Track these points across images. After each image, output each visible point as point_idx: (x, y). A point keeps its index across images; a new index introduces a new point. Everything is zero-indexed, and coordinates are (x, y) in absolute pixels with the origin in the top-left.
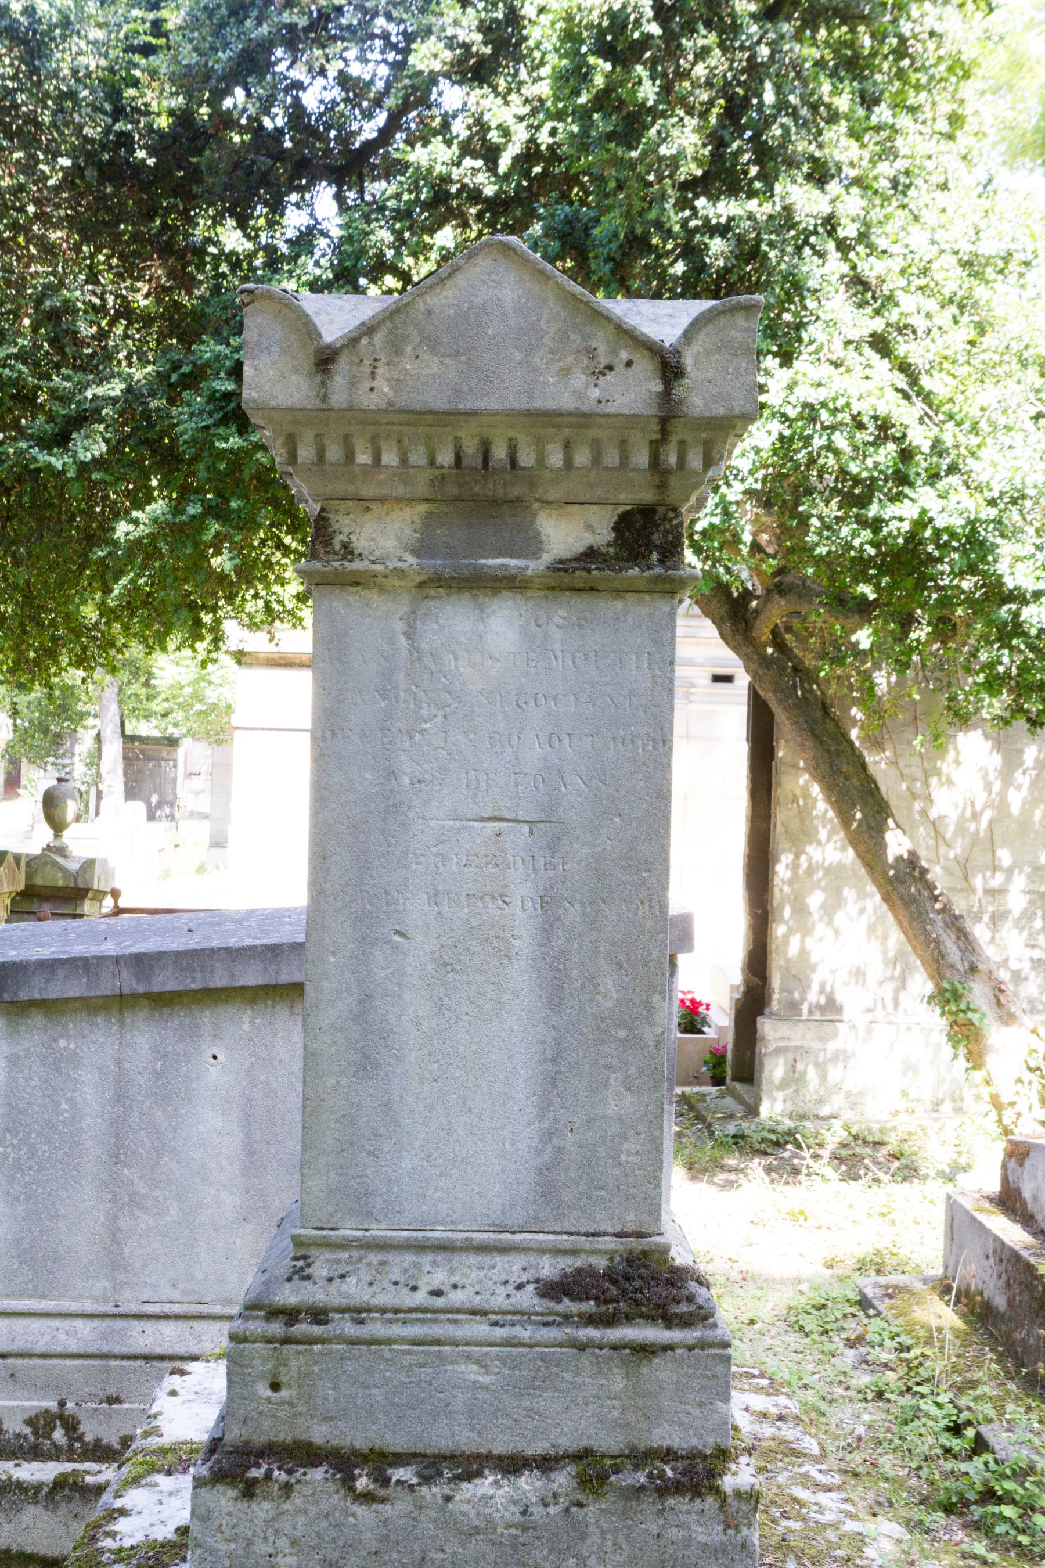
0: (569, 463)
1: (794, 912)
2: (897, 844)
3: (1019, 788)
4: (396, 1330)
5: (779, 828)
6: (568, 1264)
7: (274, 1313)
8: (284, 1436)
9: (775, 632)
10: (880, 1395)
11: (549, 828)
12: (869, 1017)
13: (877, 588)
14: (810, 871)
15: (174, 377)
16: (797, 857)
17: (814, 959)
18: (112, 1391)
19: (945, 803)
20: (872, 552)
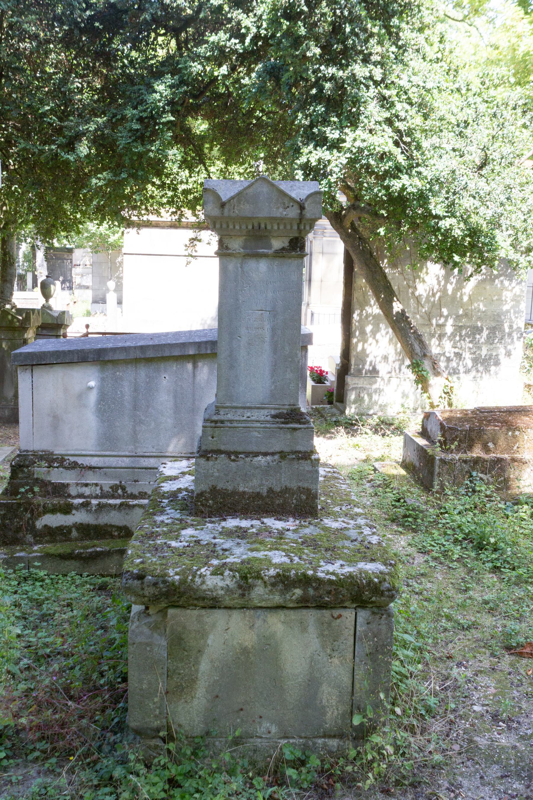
0: (278, 228)
1: (360, 333)
2: (397, 307)
3: (451, 284)
4: (240, 425)
5: (355, 300)
6: (277, 411)
7: (212, 422)
8: (215, 448)
9: (352, 224)
10: (376, 494)
11: (274, 313)
12: (389, 375)
13: (388, 211)
14: (367, 316)
15: (114, 120)
16: (362, 311)
17: (368, 352)
18: (136, 478)
19: (421, 289)
20: (385, 199)
